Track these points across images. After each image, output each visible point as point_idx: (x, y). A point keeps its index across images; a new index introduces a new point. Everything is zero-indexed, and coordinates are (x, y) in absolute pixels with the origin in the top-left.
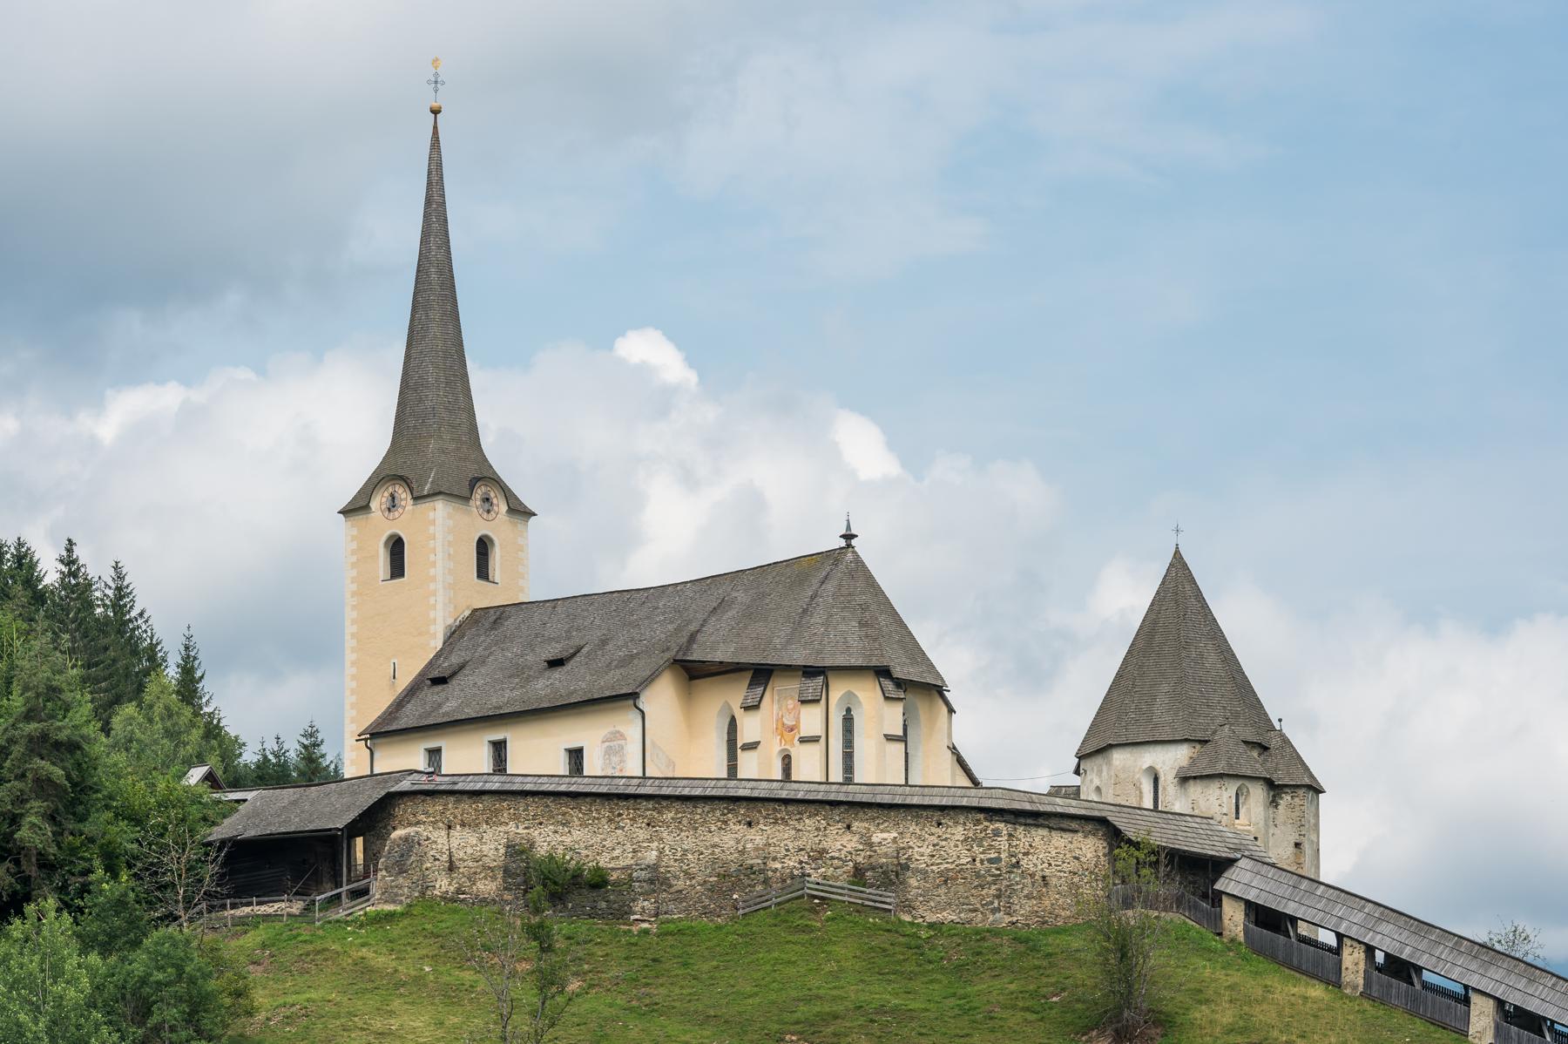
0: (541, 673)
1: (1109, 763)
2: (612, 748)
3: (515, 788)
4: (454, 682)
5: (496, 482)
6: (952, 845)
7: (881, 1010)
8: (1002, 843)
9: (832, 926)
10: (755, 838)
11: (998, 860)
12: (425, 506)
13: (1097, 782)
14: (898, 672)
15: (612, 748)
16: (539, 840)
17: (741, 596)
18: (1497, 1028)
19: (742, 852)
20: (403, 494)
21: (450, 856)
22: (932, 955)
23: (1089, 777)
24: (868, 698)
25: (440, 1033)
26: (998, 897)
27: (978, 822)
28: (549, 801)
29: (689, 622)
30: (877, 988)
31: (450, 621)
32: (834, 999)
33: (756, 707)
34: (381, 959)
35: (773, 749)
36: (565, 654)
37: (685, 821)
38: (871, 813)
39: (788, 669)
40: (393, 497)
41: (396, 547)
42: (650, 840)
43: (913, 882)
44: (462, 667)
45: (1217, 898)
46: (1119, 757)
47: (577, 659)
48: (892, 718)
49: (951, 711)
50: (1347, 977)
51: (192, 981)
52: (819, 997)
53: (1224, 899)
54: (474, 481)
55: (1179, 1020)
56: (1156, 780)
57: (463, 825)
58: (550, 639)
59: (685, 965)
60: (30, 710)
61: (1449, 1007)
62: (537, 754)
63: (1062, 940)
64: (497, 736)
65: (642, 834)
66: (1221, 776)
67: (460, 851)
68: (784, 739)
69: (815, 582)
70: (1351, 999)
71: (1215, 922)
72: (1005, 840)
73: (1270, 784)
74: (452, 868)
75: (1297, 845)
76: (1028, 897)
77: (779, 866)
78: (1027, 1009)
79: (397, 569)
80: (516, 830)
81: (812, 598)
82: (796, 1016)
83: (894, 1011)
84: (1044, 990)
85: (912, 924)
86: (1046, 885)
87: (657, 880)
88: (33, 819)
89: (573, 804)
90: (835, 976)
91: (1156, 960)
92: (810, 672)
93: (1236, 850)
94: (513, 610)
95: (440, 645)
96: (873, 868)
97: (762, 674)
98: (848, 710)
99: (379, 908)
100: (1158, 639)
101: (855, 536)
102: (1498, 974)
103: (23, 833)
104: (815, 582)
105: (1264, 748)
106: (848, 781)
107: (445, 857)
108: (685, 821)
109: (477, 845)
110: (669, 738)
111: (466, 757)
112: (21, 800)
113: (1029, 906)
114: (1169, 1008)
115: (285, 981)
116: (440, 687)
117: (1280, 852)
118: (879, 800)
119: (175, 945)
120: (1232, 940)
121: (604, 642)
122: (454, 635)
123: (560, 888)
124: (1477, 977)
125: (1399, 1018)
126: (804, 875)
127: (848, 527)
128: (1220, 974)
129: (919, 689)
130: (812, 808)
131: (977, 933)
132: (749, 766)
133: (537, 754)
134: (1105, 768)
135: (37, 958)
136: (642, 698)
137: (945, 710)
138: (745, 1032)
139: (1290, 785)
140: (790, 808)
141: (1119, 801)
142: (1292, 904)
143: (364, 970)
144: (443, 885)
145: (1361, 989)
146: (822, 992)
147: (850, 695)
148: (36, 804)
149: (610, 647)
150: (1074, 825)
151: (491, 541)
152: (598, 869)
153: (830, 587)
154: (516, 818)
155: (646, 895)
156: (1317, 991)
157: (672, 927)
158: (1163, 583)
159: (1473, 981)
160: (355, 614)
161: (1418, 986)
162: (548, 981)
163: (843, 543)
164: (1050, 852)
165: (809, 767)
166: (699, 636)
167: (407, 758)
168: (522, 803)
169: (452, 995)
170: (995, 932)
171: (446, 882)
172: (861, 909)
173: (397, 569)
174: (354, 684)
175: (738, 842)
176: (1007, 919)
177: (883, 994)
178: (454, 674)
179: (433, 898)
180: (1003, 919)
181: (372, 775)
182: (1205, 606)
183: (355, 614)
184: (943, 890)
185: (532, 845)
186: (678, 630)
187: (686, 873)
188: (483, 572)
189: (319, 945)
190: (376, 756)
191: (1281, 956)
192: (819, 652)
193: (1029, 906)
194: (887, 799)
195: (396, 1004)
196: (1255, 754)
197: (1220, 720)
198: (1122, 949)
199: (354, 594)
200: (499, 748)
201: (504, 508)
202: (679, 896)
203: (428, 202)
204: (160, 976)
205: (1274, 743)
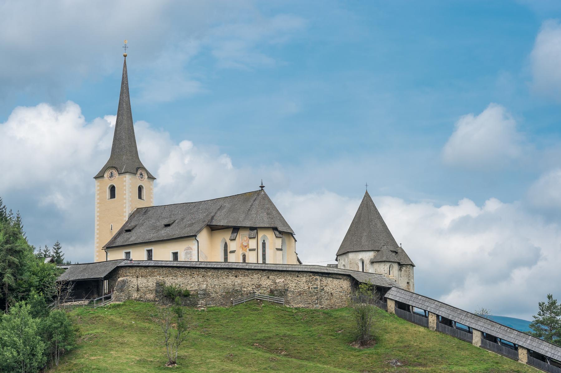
0: (162, 228)
1: (348, 257)
2: (188, 252)
3: (159, 265)
4: (133, 231)
5: (144, 168)
6: (303, 283)
7: (285, 336)
8: (318, 282)
9: (265, 309)
10: (238, 281)
11: (317, 288)
12: (122, 176)
13: (343, 263)
14: (280, 229)
15: (188, 252)
16: (167, 282)
17: (227, 205)
18: (482, 341)
19: (234, 285)
20: (115, 172)
21: (138, 286)
22: (298, 318)
23: (341, 261)
24: (270, 236)
25: (141, 343)
26: (317, 299)
27: (310, 276)
28: (170, 269)
29: (211, 213)
30: (281, 328)
31: (130, 212)
32: (269, 332)
33: (235, 240)
34: (118, 319)
35: (240, 252)
36: (170, 223)
37: (215, 276)
38: (275, 273)
39: (245, 228)
40: (112, 173)
41: (113, 189)
42: (204, 281)
43: (289, 295)
44: (135, 226)
45: (386, 300)
46: (351, 255)
47: (174, 224)
48: (278, 243)
49: (296, 241)
50: (430, 325)
51: (66, 327)
52: (263, 331)
53: (388, 300)
54: (137, 168)
55: (381, 338)
56: (363, 263)
57: (142, 277)
58: (164, 218)
59: (217, 321)
60: (7, 240)
61: (465, 334)
62: (163, 254)
63: (339, 313)
64: (149, 248)
65: (201, 280)
66: (384, 261)
67: (142, 284)
68: (243, 250)
69: (252, 201)
71: (385, 307)
72: (319, 281)
73: (399, 264)
74: (138, 290)
75: (408, 283)
76: (327, 299)
77: (245, 290)
78: (331, 335)
79: (113, 195)
80: (160, 278)
81: (251, 206)
82: (257, 338)
83: (289, 336)
84: (336, 329)
85: (290, 308)
86: (332, 296)
87: (206, 294)
88: (8, 275)
89: (178, 270)
90: (268, 324)
91: (373, 319)
92: (252, 229)
93: (391, 285)
94: (151, 209)
95: (127, 220)
96: (277, 290)
97: (236, 229)
98: (264, 241)
99: (115, 303)
100: (362, 219)
101: (264, 187)
102: (481, 324)
103: (5, 279)
104: (252, 201)
105: (396, 253)
106: (264, 262)
107: (136, 287)
108: (215, 276)
109: (148, 283)
110: (205, 249)
111: (139, 255)
112: (4, 269)
113: (327, 302)
114: (377, 335)
115: (87, 327)
116: (129, 233)
117: (403, 285)
118: (278, 269)
119: (60, 315)
120: (391, 313)
121: (183, 219)
122: (132, 216)
123: (169, 295)
124: (474, 325)
125: (449, 338)
126: (254, 293)
127: (262, 184)
128: (391, 324)
129: (286, 234)
130: (256, 272)
131: (311, 311)
132: (232, 258)
133: (163, 254)
134: (346, 259)
135: (19, 320)
136: (198, 236)
137: (294, 241)
138: (241, 343)
139: (404, 263)
140: (249, 271)
141: (351, 269)
142: (411, 302)
143: (113, 323)
144: (135, 295)
145: (435, 328)
146: (264, 330)
147: (265, 236)
148: (9, 270)
149: (185, 220)
150: (340, 277)
151: (142, 187)
152: (187, 290)
153: (257, 202)
154: (159, 274)
155: (203, 299)
156: (422, 329)
157: (212, 309)
158: (363, 201)
159: (473, 326)
160: (98, 210)
161: (455, 328)
162: (182, 327)
163: (260, 189)
164: (332, 285)
165: (252, 258)
166: (215, 218)
167: (119, 255)
168: (161, 270)
169: (143, 331)
170: (316, 311)
171: (136, 294)
172: (273, 303)
173: (113, 195)
174: (98, 231)
175: (232, 282)
176: (320, 306)
177: (283, 330)
178: (133, 228)
179: (132, 299)
180: (319, 306)
181: (107, 261)
182: (376, 209)
183: (98, 210)
184: (299, 297)
185: (165, 283)
186: (207, 215)
187: (215, 292)
188: (140, 197)
189: (96, 315)
190: (108, 254)
191: (413, 320)
192: (255, 222)
193: (327, 302)
194: (281, 269)
195: (125, 334)
196: (394, 254)
197: (382, 244)
198: (363, 316)
199: (98, 203)
200: (150, 252)
201: (146, 177)
202: (213, 299)
203: (123, 83)
204: (56, 325)
205: (399, 251)
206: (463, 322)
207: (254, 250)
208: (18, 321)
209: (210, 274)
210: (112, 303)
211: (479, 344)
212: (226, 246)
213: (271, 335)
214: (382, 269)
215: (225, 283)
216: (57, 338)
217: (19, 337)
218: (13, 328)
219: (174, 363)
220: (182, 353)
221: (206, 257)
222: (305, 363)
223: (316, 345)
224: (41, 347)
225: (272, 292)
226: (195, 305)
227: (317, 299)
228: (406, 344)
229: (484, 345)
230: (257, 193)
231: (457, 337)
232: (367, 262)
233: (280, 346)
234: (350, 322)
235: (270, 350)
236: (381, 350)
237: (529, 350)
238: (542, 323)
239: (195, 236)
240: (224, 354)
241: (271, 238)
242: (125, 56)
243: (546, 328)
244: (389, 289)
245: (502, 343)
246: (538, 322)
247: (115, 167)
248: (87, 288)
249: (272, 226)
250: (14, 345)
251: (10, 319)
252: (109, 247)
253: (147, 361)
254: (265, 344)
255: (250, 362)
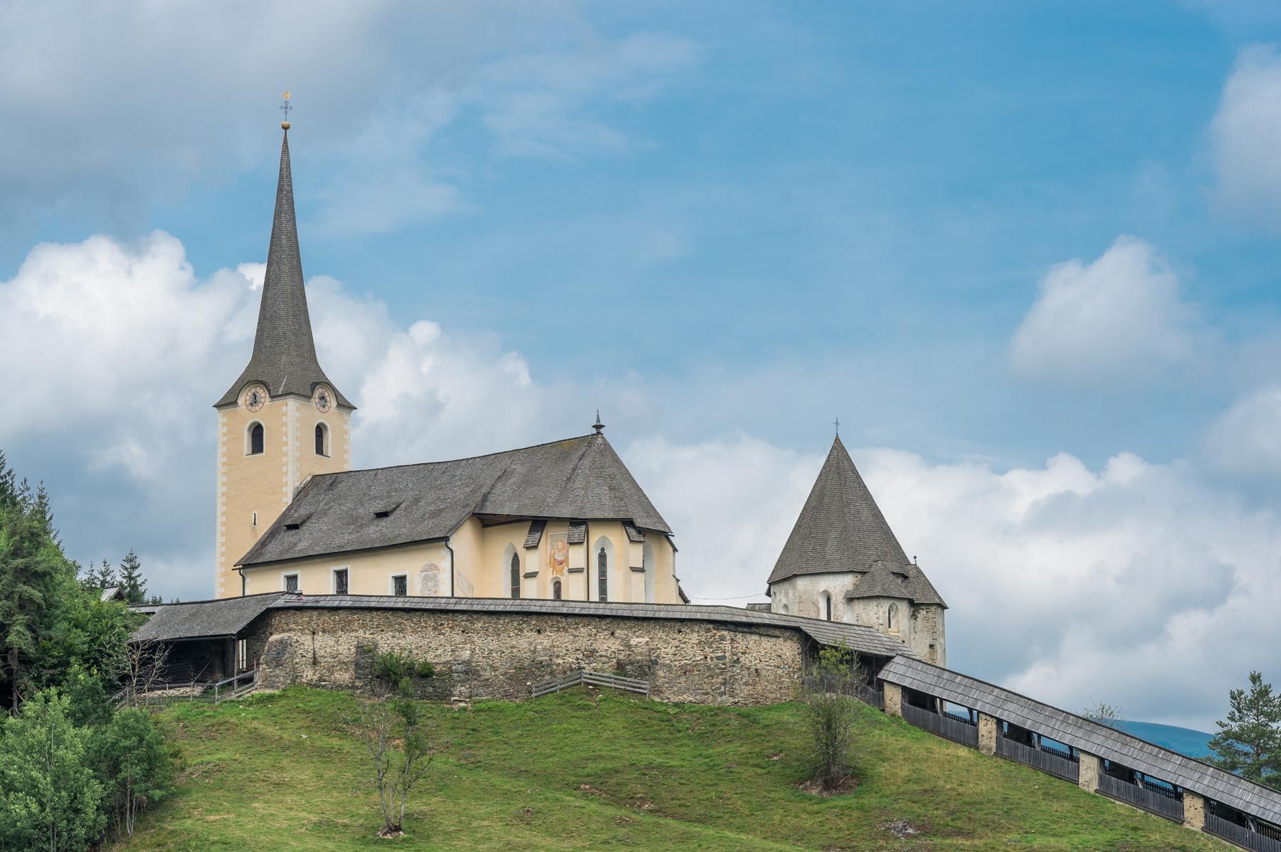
0: (371, 521)
1: (794, 588)
2: (430, 577)
3: (363, 605)
4: (304, 528)
5: (328, 385)
6: (691, 645)
7: (650, 766)
8: (727, 645)
9: (604, 706)
10: (544, 641)
11: (724, 657)
12: (278, 402)
13: (784, 601)
14: (640, 522)
15: (430, 577)
16: (381, 643)
17: (519, 468)
18: (1101, 779)
19: (534, 651)
20: (262, 393)
21: (314, 653)
22: (680, 726)
23: (778, 597)
24: (616, 540)
25: (321, 784)
26: (724, 684)
27: (708, 630)
28: (388, 614)
29: (481, 486)
30: (643, 750)
31: (297, 484)
32: (613, 758)
33: (536, 547)
34: (270, 729)
35: (548, 577)
36: (389, 509)
37: (491, 630)
38: (629, 624)
39: (559, 521)
40: (255, 396)
41: (257, 433)
42: (465, 643)
43: (661, 673)
44: (309, 517)
45: (880, 684)
46: (801, 584)
47: (397, 512)
48: (636, 554)
49: (675, 550)
50: (983, 742)
51: (150, 747)
52: (601, 757)
53: (886, 686)
54: (313, 385)
55: (869, 773)
56: (829, 600)
57: (324, 632)
58: (375, 498)
59: (497, 733)
60: (16, 549)
61: (1063, 764)
62: (372, 580)
63: (774, 715)
64: (341, 567)
65: (458, 638)
66: (878, 597)
67: (325, 649)
68: (554, 570)
69: (575, 458)
70: (983, 756)
71: (879, 701)
72: (728, 643)
73: (911, 603)
74: (315, 662)
75: (931, 646)
76: (746, 684)
77: (561, 661)
78: (756, 765)
79: (257, 446)
80: (364, 635)
81: (574, 470)
82: (586, 771)
83: (659, 767)
84: (767, 752)
85: (661, 704)
86: (758, 675)
87: (470, 671)
88: (18, 628)
89: (407, 617)
90: (611, 741)
91: (852, 729)
92: (575, 522)
93: (892, 650)
94: (344, 476)
95: (290, 502)
96: (632, 663)
97: (538, 524)
98: (603, 550)
99: (262, 691)
100: (826, 500)
101: (602, 426)
102: (1099, 740)
103: (12, 638)
104: (575, 458)
105: (905, 577)
106: (603, 599)
107: (310, 655)
108: (491, 630)
109: (338, 645)
110: (468, 569)
111: (317, 583)
112: (9, 614)
113: (747, 690)
114: (861, 765)
115: (198, 746)
116: (293, 532)
117: (921, 651)
118: (635, 614)
119: (137, 720)
120: (893, 715)
121: (417, 500)
122: (301, 494)
123: (386, 675)
124: (1083, 741)
125: (1026, 771)
126: (580, 668)
127: (598, 420)
128: (892, 739)
129: (652, 534)
130: (586, 620)
131: (711, 710)
132: (530, 590)
133: (372, 580)
134: (791, 592)
135: (43, 730)
136: (451, 540)
137: (671, 549)
138: (550, 783)
139: (923, 601)
140: (569, 620)
141: (802, 615)
142: (938, 689)
143: (257, 738)
144: (309, 674)
145: (994, 750)
146: (603, 753)
147: (604, 538)
148: (21, 618)
149: (422, 503)
150: (777, 633)
151: (325, 427)
152: (426, 663)
153: (586, 462)
154: (364, 626)
155: (463, 682)
156: (963, 752)
157: (483, 705)
158: (828, 460)
159: (1080, 744)
160: (225, 479)
161: (1038, 749)
162: (415, 748)
163: (594, 431)
164: (758, 651)
165: (575, 590)
166: (491, 497)
167: (271, 583)
168: (368, 616)
169: (326, 756)
170: (723, 709)
171: (310, 673)
172: (623, 693)
173: (257, 446)
174: (224, 529)
175: (530, 644)
176: (731, 700)
177: (647, 754)
178: (304, 522)
179: (302, 684)
180: (727, 700)
181: (244, 597)
182: (858, 477)
183: (225, 479)
184: (683, 679)
185: (376, 646)
186: (473, 492)
187: (491, 666)
188: (320, 450)
189: (220, 718)
190: (247, 580)
191: (942, 731)
192: (582, 508)
193: (747, 690)
194: (641, 614)
195: (285, 762)
196: (899, 581)
197: (873, 558)
198: (828, 723)
199: (224, 464)
200: (342, 576)
201: (334, 404)
202: (486, 683)
203: (280, 190)
204: (127, 743)
205: (911, 574)
206: (1058, 735)
207: (579, 571)
208: (40, 733)
209: (479, 625)
210: (257, 691)
211: (1094, 786)
212: (516, 561)
213: (618, 765)
214: (872, 614)
215: (513, 647)
216: (131, 771)
217: (44, 769)
218: (29, 750)
219: (398, 829)
220: (417, 806)
221: (471, 587)
222: (696, 829)
223: (722, 787)
224: (93, 793)
225: (620, 667)
226: (444, 696)
227: (724, 684)
228: (927, 786)
229: (1104, 789)
230: (587, 441)
231: (1043, 771)
232: (838, 599)
233: (640, 790)
234: (800, 737)
235: (617, 799)
236: (870, 800)
237: (1207, 800)
238: (1238, 737)
239: (446, 539)
240: (513, 809)
241: (618, 544)
242: (286, 128)
243: (1247, 749)
244: (889, 659)
245: (1147, 784)
246: (1228, 735)
247: (262, 382)
248: (199, 657)
249: (622, 516)
250: (32, 788)
251: (23, 730)
252: (249, 565)
253: (336, 825)
254: (606, 785)
255: (571, 826)
